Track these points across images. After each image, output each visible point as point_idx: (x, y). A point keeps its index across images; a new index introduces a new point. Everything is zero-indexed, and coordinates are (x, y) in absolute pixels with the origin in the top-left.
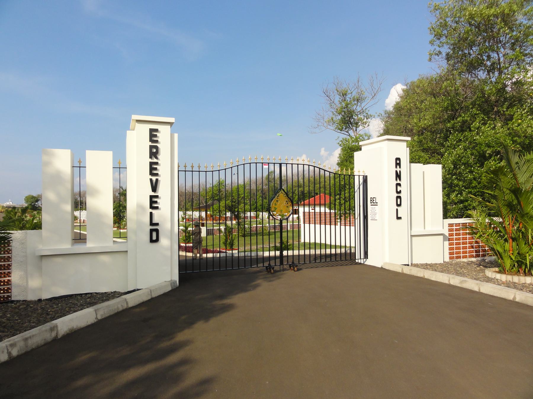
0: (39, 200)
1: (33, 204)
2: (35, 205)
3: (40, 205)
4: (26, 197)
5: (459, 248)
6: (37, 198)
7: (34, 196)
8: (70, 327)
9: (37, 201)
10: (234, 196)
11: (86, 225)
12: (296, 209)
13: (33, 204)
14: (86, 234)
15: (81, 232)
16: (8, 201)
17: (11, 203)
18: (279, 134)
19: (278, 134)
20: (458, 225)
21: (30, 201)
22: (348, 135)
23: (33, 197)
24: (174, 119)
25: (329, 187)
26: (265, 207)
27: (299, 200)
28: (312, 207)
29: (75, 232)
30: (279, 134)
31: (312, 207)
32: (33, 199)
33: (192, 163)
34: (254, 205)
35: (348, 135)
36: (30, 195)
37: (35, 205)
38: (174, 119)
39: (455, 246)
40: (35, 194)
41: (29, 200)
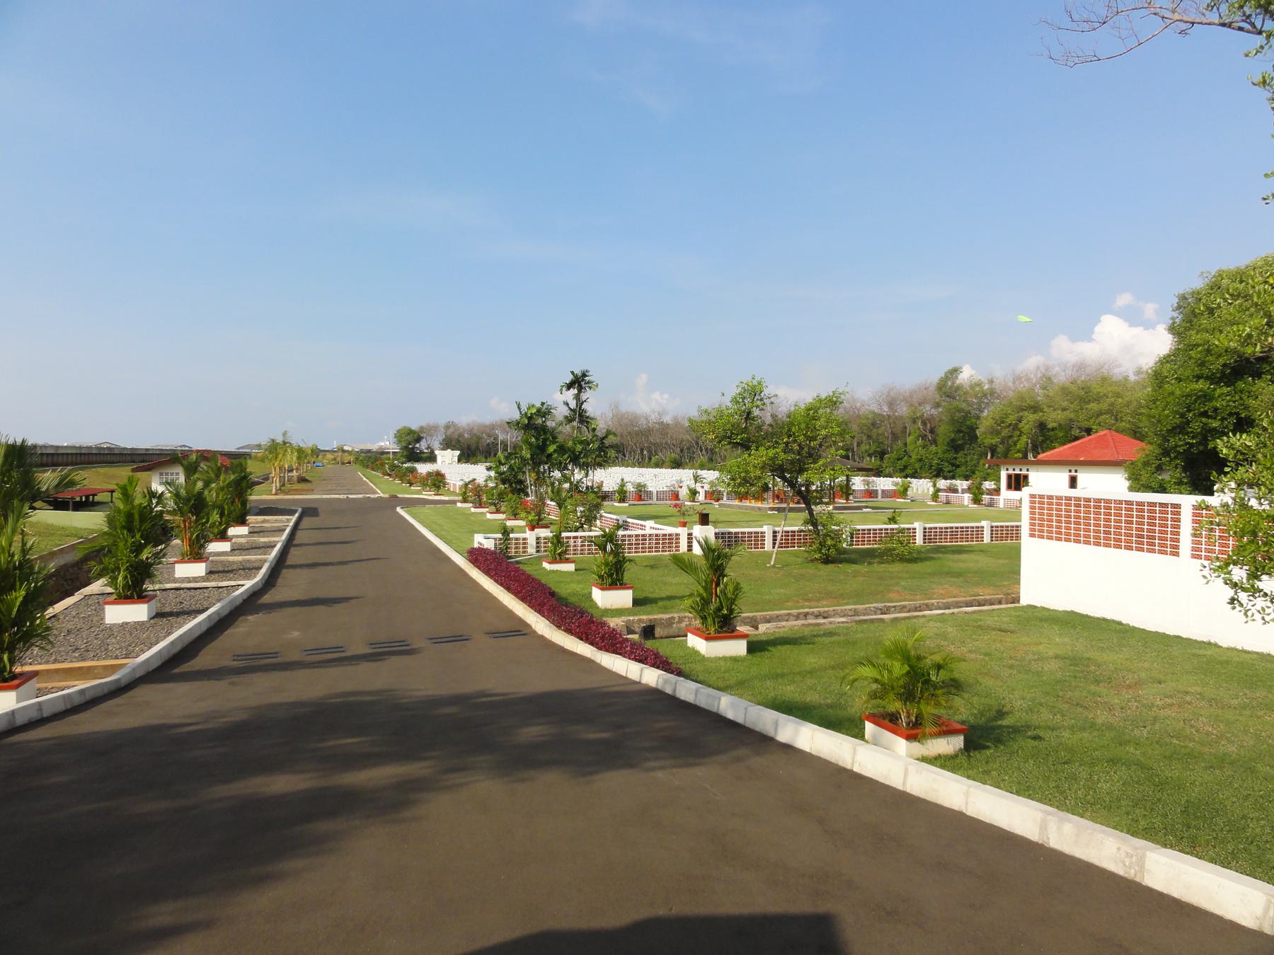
0: (423, 438)
1: (410, 446)
3: (424, 448)
4: (398, 431)
5: (1040, 525)
7: (413, 429)
9: (418, 440)
10: (794, 434)
12: (1020, 475)
13: (410, 446)
16: (383, 440)
17: (388, 443)
20: (1118, 502)
22: (1167, 18)
23: (410, 432)
26: (931, 466)
27: (1037, 447)
28: (1007, 470)
31: (1007, 470)
32: (411, 435)
33: (561, 393)
34: (901, 459)
35: (1167, 18)
36: (405, 428)
37: (414, 448)
39: (1037, 522)
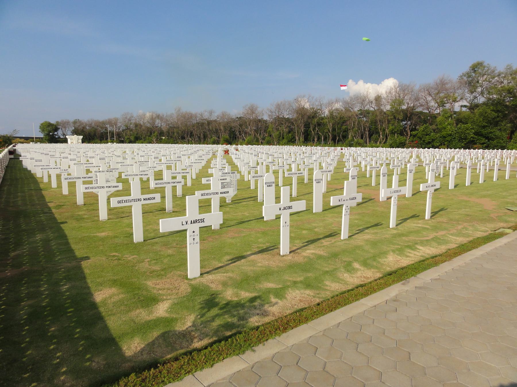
1: (51, 134)
2: (53, 135)
4: (42, 124)
6: (56, 126)
8: (473, 63)
9: (56, 129)
11: (155, 180)
14: (392, 188)
15: (282, 188)
18: (365, 39)
19: (363, 38)
21: (46, 130)
23: (50, 125)
24: (342, 89)
25: (411, 252)
29: (344, 182)
30: (365, 39)
36: (46, 122)
37: (53, 135)
38: (342, 89)
40: (53, 122)
41: (46, 129)
